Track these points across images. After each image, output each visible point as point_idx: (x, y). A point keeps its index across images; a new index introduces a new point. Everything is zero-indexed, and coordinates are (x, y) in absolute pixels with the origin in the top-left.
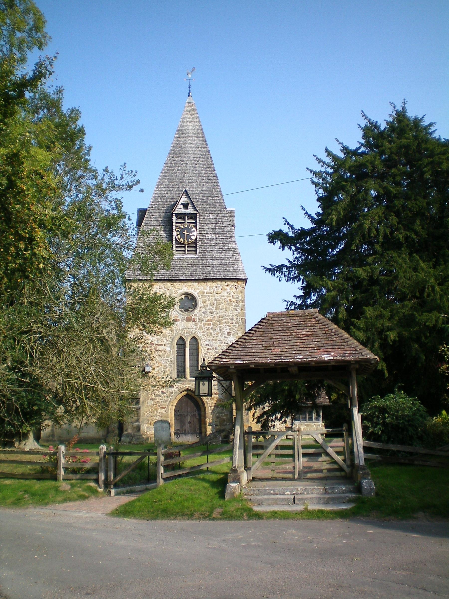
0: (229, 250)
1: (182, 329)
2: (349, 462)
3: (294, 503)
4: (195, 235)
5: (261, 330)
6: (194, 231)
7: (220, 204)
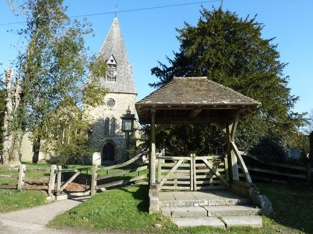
2: (228, 179)
3: (208, 216)
4: (115, 74)
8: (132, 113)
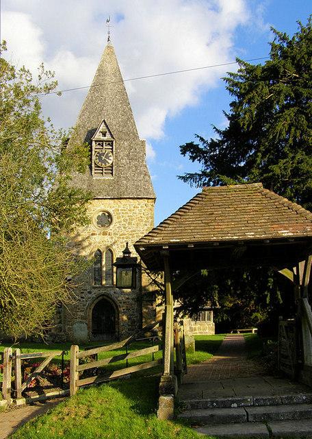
0: (141, 173)
1: (99, 243)
5: (198, 205)
6: (110, 156)
7: (134, 134)
8: (132, 256)
